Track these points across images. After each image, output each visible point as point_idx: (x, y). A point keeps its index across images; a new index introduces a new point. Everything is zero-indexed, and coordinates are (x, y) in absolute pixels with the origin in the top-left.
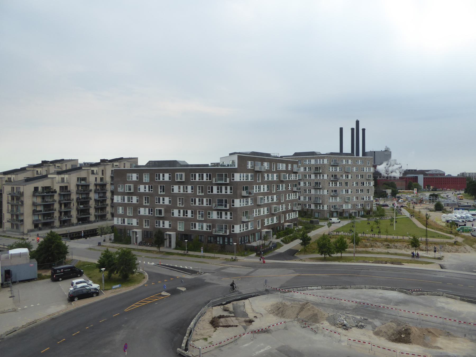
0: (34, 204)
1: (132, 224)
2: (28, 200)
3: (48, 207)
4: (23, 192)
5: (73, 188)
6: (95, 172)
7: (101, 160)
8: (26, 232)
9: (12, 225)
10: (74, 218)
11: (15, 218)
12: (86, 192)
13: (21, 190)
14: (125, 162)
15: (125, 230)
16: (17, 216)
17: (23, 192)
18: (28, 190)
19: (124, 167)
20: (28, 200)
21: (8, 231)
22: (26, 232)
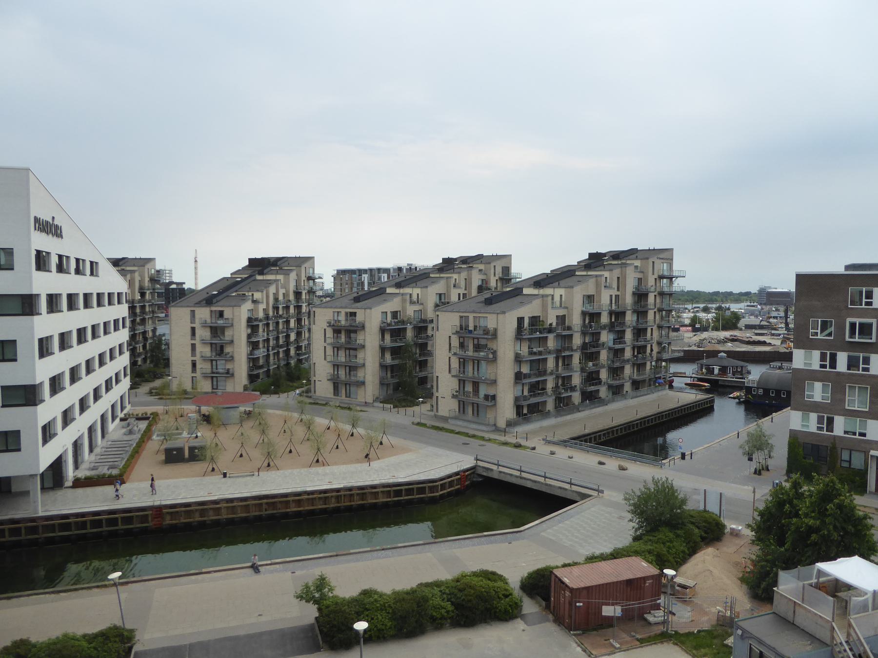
0: (518, 359)
1: (864, 435)
2: (507, 348)
3: (538, 365)
4: (496, 330)
5: (576, 321)
6: (415, 298)
7: (590, 254)
8: (502, 424)
9: (462, 406)
10: (3, 342)
11: (469, 388)
12: (538, 334)
13: (491, 325)
14: (655, 259)
15: (834, 448)
16: (476, 385)
17: (496, 330)
18: (505, 322)
19: (193, 312)
20: (507, 348)
21: (452, 418)
22: (502, 424)
